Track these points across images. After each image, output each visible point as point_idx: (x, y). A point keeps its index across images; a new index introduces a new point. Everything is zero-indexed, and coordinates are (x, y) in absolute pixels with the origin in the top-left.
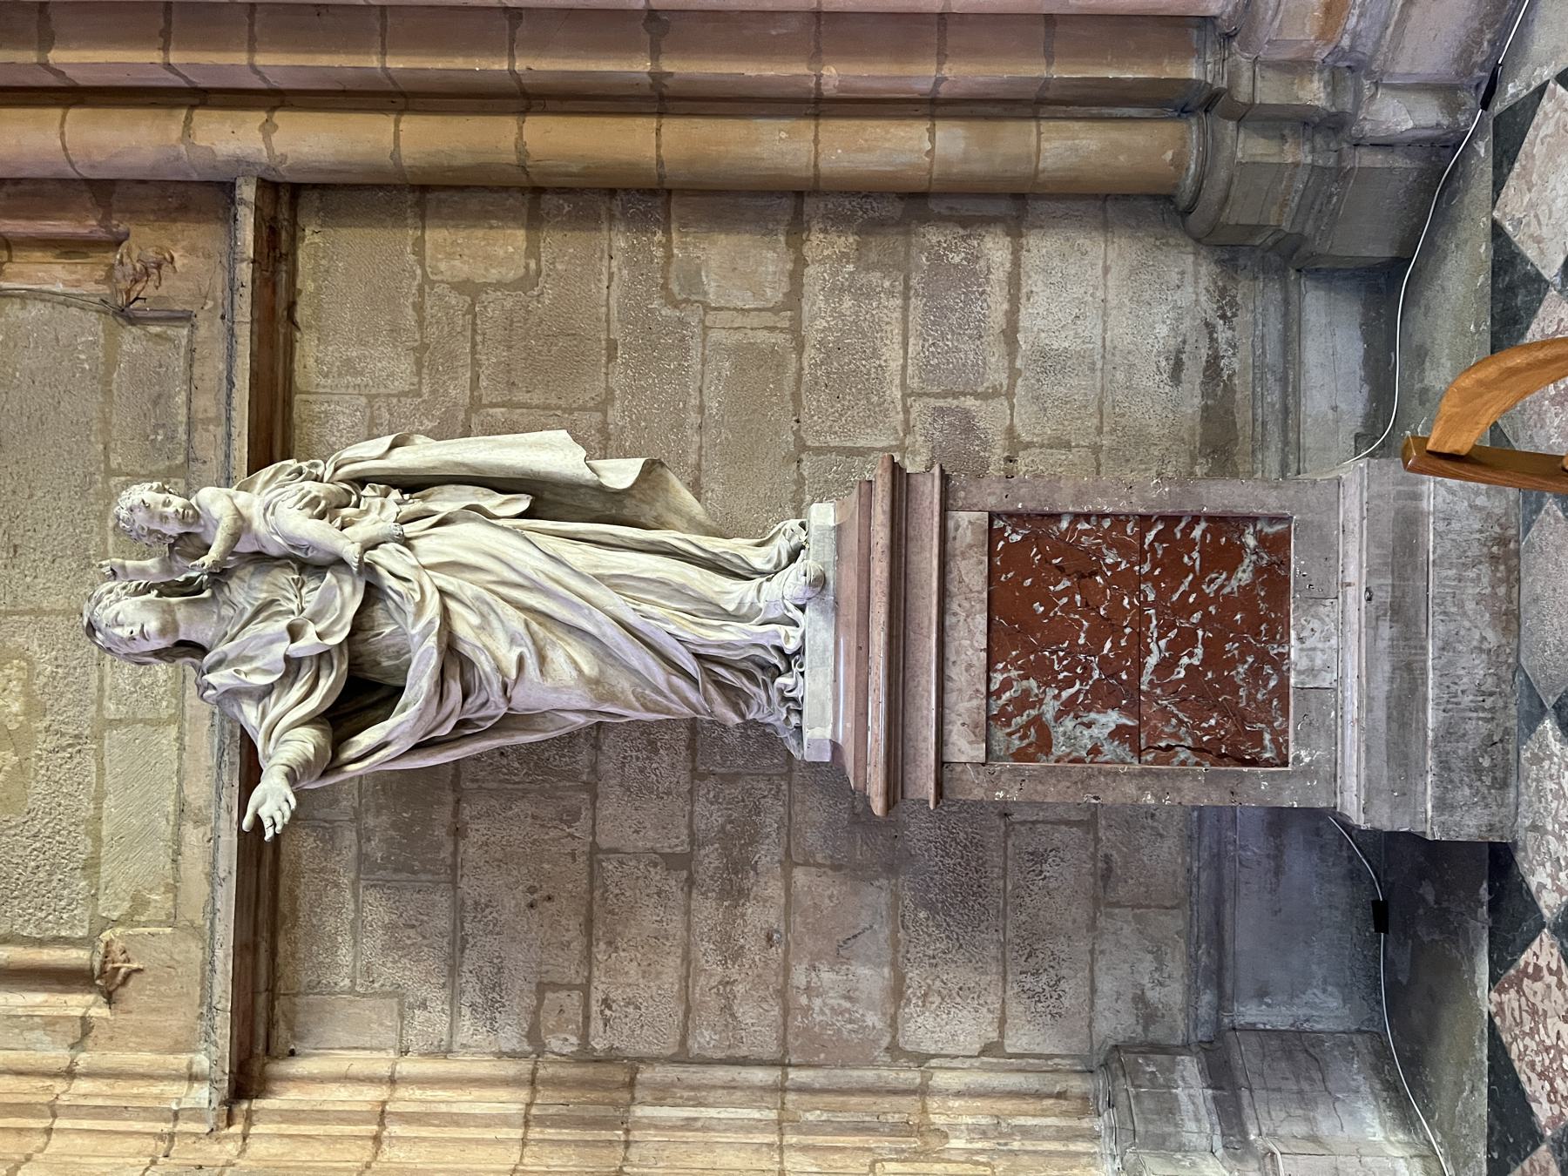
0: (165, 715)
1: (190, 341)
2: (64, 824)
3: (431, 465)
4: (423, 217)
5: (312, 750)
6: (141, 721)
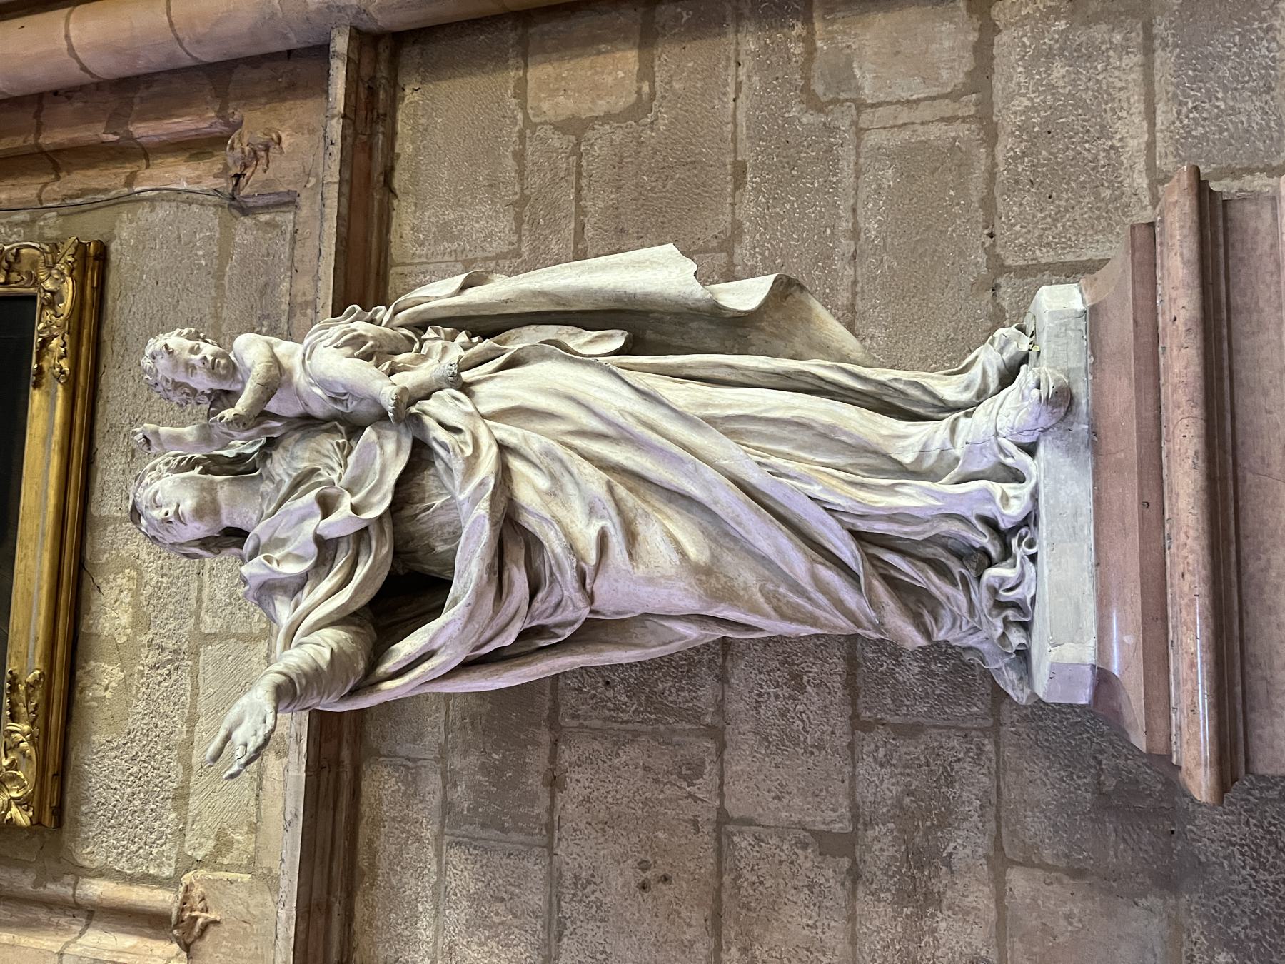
0: (256, 630)
2: (159, 748)
3: (504, 298)
4: (525, 56)
5: (327, 655)
6: (234, 636)
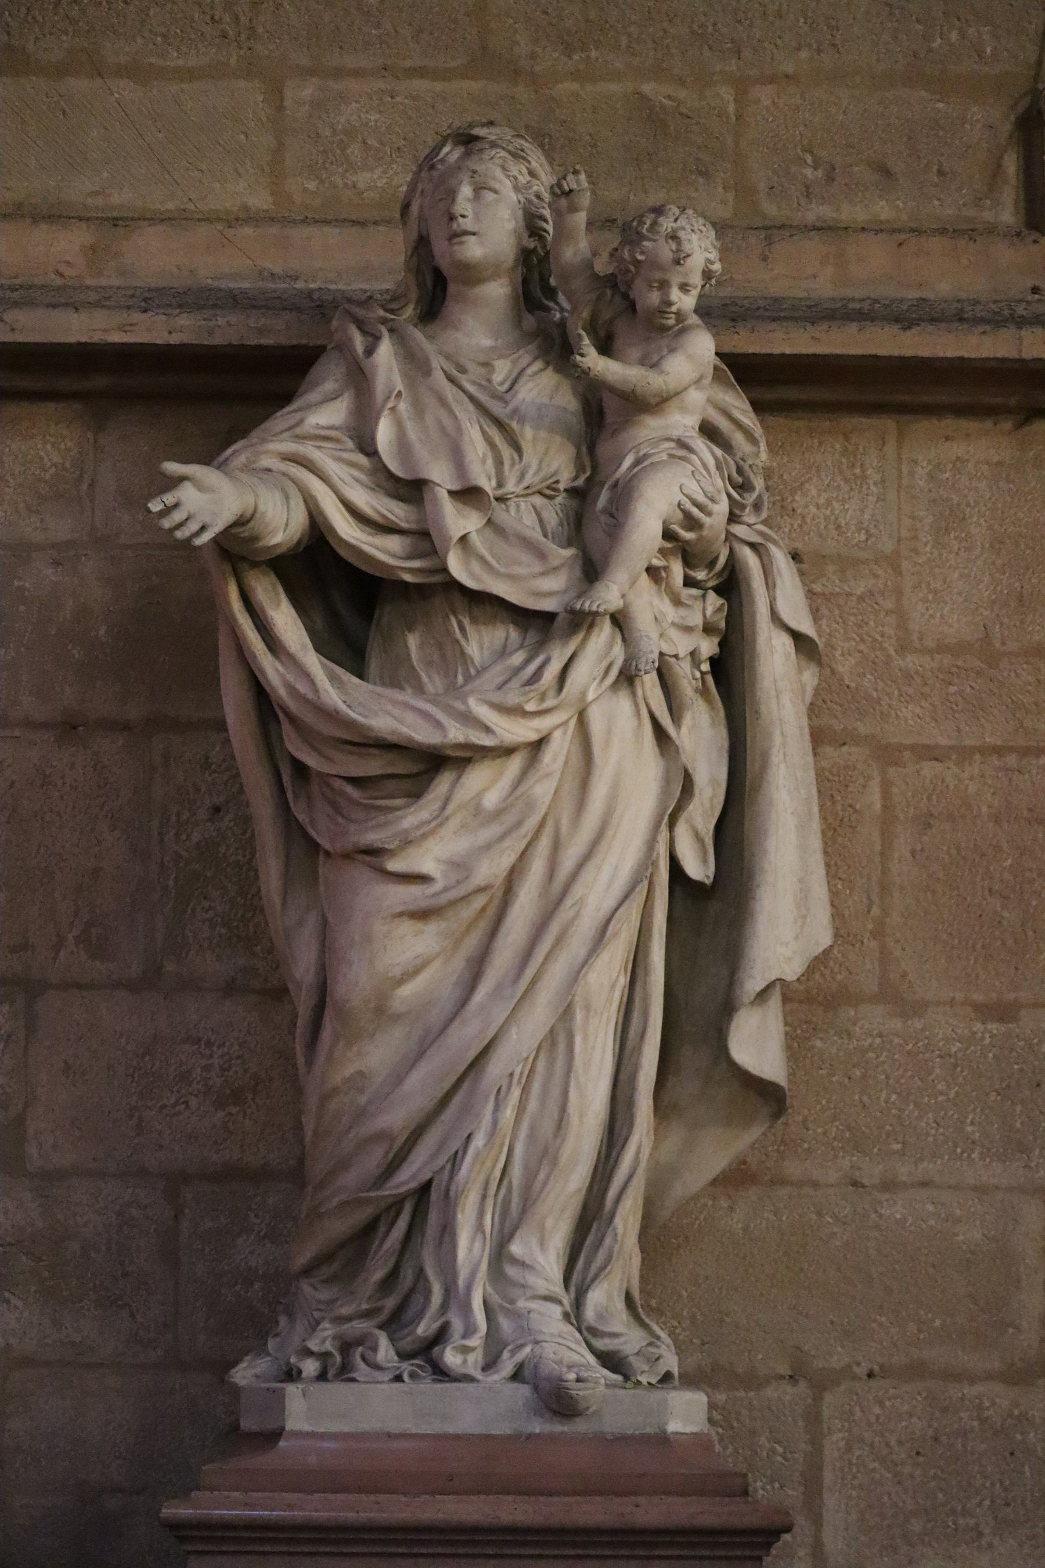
1: (991, 230)
